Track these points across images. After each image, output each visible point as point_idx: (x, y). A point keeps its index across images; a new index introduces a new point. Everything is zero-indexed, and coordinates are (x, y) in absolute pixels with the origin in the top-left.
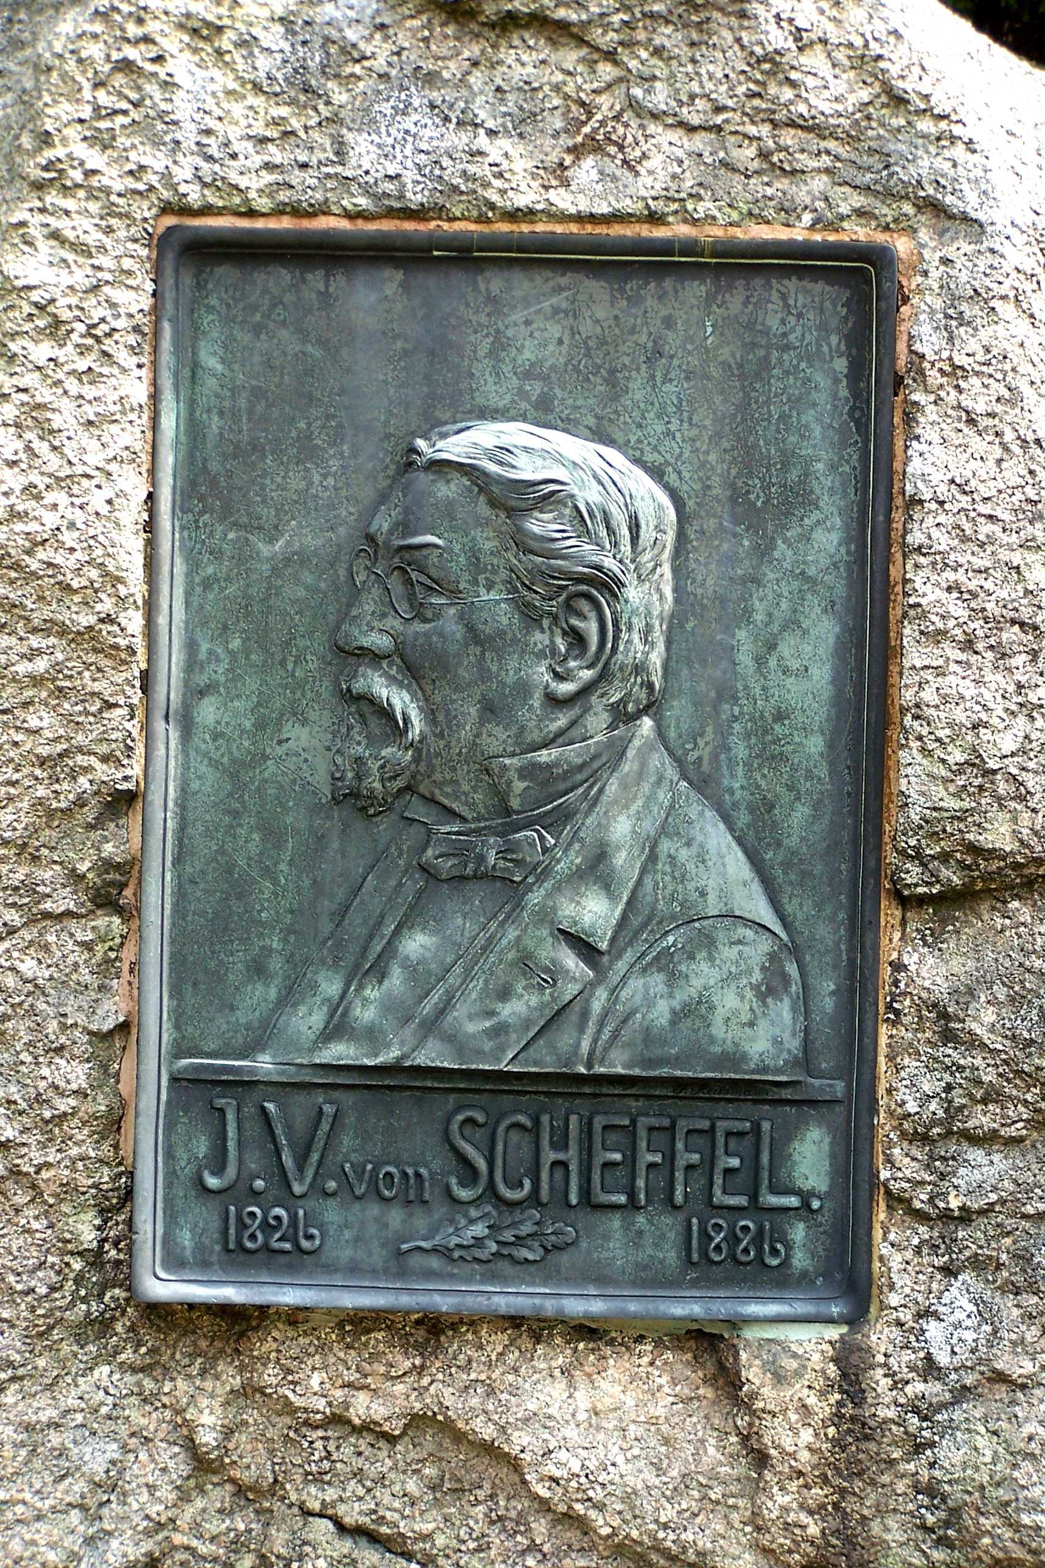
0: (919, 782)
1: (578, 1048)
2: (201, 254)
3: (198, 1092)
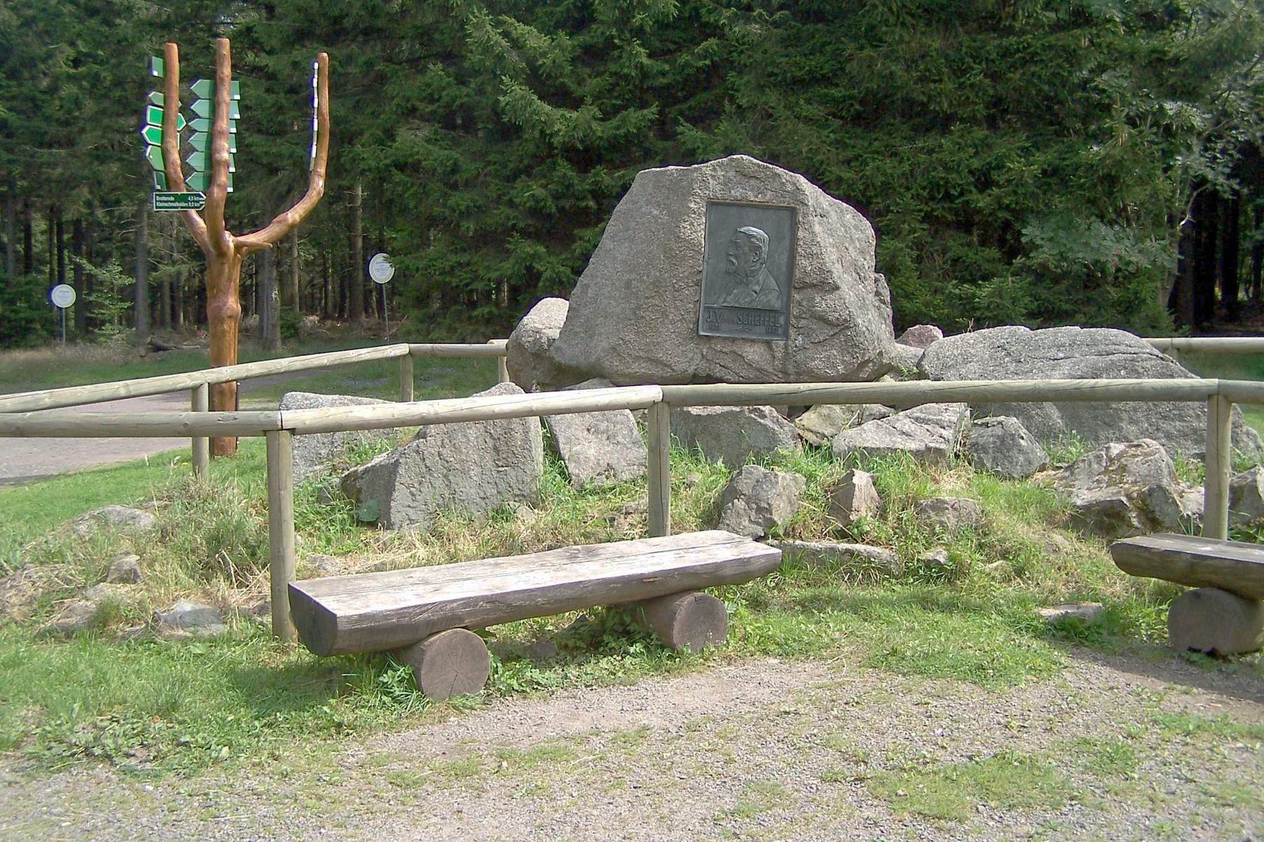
0: (798, 274)
1: (754, 305)
2: (712, 204)
3: (708, 309)
